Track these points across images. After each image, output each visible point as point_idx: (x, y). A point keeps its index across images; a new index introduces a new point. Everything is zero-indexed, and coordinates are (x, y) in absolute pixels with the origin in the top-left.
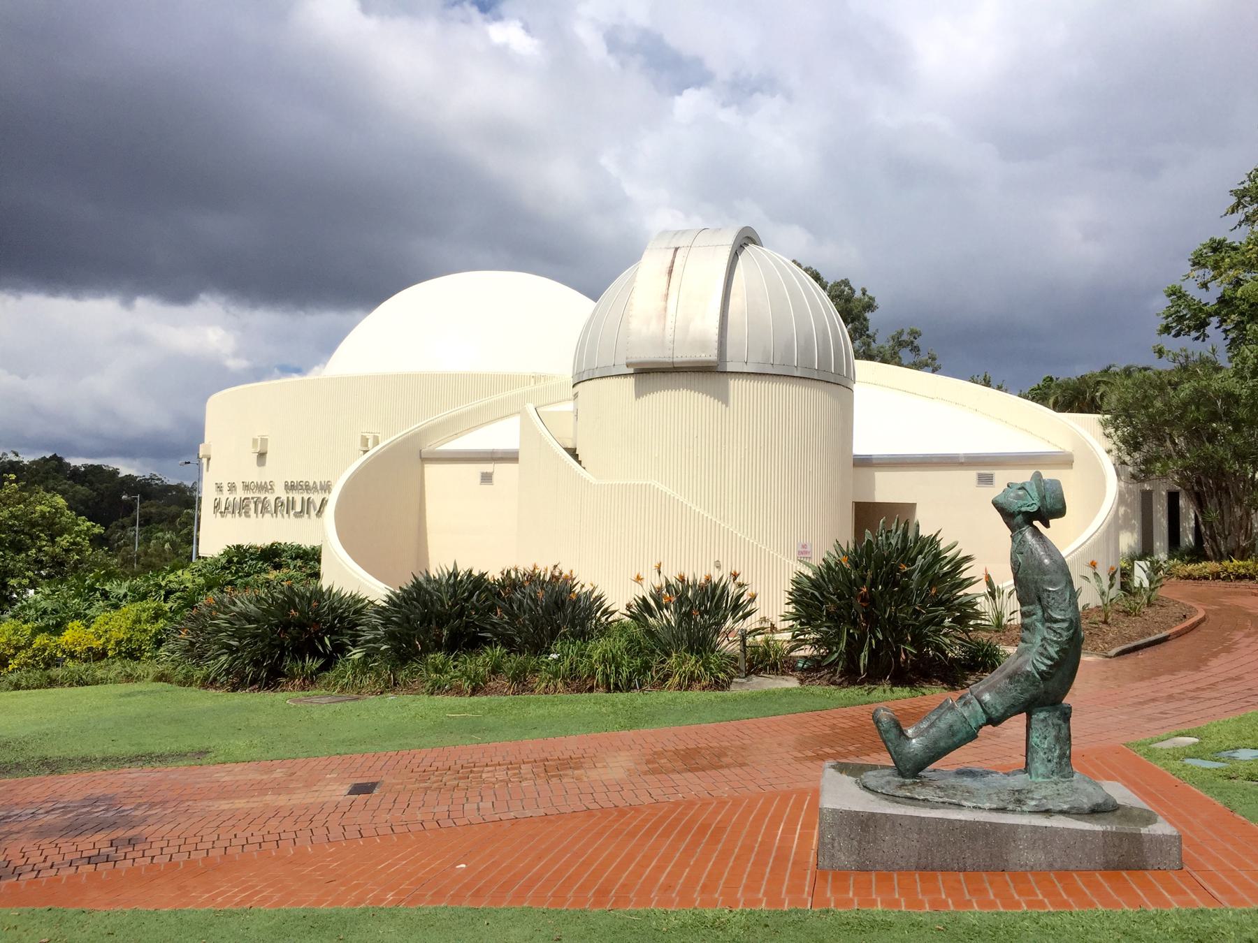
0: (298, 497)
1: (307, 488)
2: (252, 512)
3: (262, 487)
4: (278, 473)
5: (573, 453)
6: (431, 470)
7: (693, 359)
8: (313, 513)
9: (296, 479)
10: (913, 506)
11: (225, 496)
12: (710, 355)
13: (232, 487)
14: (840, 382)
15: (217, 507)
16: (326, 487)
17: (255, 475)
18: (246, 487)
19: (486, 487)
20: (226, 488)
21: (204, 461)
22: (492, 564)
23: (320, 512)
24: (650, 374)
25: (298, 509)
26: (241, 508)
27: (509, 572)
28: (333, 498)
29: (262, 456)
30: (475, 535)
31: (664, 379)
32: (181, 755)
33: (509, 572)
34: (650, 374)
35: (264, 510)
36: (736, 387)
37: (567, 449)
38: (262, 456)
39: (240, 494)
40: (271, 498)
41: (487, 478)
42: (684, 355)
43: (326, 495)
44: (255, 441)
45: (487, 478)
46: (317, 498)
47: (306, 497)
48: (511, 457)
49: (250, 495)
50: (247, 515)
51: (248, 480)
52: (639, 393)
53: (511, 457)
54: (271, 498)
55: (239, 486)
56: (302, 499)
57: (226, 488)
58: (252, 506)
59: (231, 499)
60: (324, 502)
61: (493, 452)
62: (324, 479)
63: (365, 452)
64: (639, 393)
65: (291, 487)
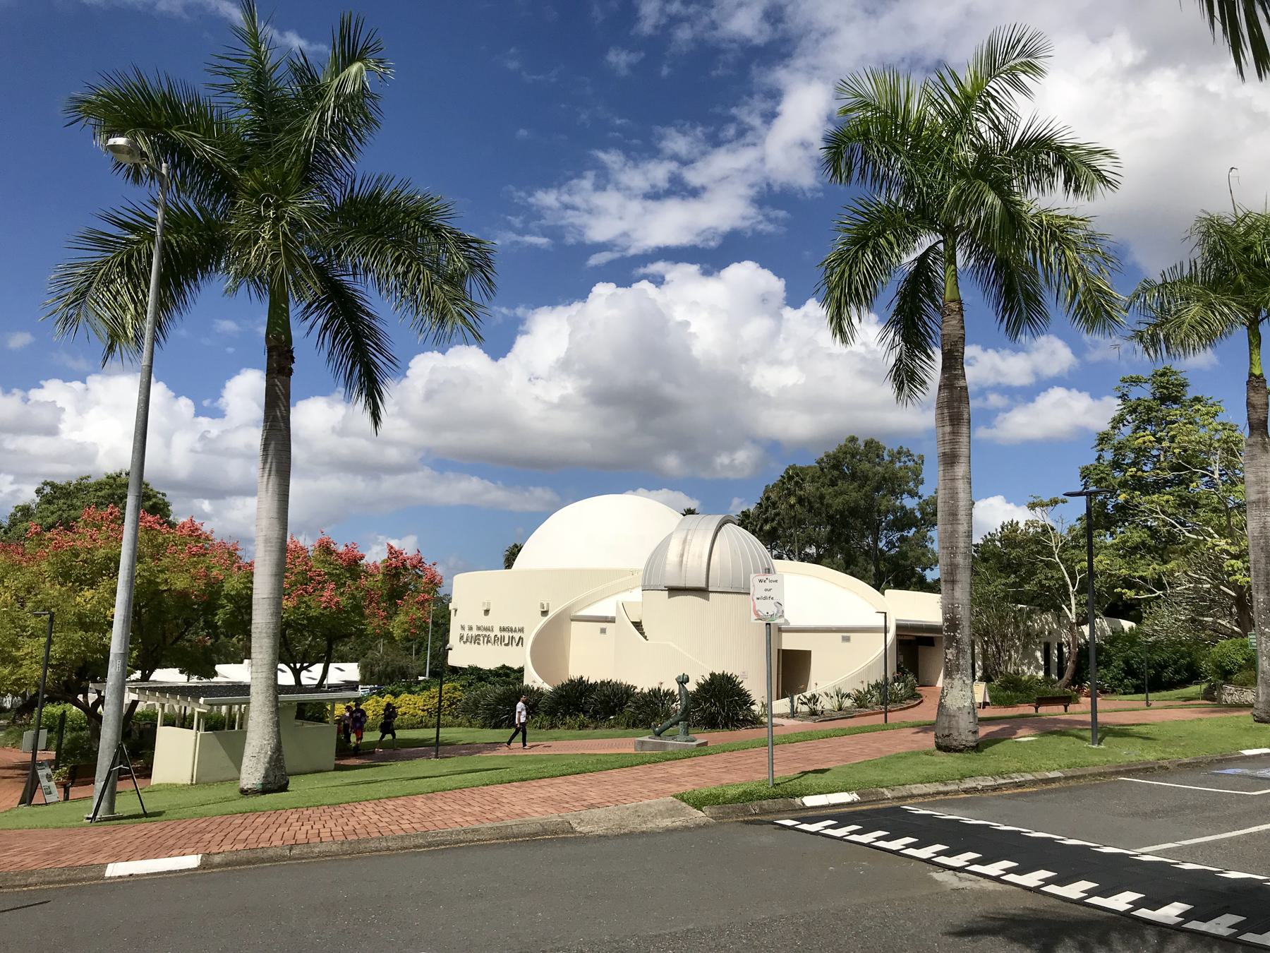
0: (506, 635)
1: (511, 630)
3: (487, 629)
4: (495, 621)
5: (638, 625)
6: (784, 635)
10: (810, 652)
11: (466, 633)
12: (703, 585)
13: (471, 628)
15: (461, 638)
16: (521, 630)
18: (479, 628)
19: (847, 644)
22: (593, 677)
24: (674, 591)
26: (476, 640)
29: (487, 612)
30: (590, 660)
34: (674, 591)
37: (633, 623)
38: (487, 612)
39: (475, 632)
40: (492, 635)
41: (603, 631)
42: (690, 584)
45: (603, 631)
46: (517, 636)
48: (612, 620)
53: (612, 620)
54: (492, 635)
56: (511, 637)
62: (518, 626)
65: (503, 629)
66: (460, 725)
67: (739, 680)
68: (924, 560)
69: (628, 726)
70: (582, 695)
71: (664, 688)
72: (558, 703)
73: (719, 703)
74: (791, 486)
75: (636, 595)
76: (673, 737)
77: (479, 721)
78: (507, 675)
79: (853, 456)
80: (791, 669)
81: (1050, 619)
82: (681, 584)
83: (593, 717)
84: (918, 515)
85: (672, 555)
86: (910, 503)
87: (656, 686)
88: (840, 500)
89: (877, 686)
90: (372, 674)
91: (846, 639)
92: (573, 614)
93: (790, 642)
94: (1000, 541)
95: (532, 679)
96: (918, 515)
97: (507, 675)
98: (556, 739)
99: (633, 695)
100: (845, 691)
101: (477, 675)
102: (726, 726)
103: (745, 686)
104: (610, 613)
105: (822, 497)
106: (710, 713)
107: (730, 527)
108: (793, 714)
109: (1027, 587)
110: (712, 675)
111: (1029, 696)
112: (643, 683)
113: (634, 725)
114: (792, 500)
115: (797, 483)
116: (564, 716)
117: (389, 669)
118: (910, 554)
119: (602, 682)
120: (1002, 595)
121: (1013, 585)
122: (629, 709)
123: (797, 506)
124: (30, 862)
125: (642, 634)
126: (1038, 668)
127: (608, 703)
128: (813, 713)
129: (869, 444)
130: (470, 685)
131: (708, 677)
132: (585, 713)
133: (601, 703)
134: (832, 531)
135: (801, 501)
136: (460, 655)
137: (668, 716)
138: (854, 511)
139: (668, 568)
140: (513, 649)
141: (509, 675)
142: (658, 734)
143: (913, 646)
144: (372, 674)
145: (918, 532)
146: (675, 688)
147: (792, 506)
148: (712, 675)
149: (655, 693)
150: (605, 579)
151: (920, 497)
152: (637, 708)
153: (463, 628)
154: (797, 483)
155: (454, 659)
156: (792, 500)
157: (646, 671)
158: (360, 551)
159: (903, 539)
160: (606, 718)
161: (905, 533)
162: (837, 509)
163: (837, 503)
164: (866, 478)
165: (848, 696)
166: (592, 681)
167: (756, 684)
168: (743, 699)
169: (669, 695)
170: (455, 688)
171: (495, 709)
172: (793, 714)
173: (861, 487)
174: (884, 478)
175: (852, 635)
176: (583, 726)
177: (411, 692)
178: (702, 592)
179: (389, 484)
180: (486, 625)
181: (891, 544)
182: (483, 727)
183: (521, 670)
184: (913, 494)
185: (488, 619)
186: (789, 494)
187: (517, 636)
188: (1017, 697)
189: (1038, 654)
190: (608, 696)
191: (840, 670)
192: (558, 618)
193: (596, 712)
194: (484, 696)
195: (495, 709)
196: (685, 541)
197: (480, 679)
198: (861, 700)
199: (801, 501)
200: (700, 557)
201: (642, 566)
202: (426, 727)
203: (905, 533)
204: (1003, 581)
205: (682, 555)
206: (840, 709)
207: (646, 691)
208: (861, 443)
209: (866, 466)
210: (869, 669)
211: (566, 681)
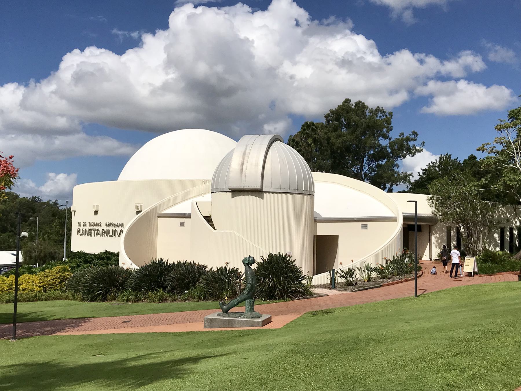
0: (111, 229)
1: (114, 225)
2: (93, 234)
3: (97, 225)
4: (102, 219)
5: (208, 219)
6: (318, 224)
7: (254, 187)
8: (117, 235)
9: (110, 222)
11: (82, 228)
12: (258, 186)
13: (85, 225)
14: (307, 192)
15: (79, 232)
16: (122, 225)
17: (96, 219)
18: (90, 224)
19: (182, 228)
20: (82, 225)
21: (73, 213)
23: (119, 236)
24: (236, 192)
25: (111, 234)
26: (88, 233)
27: (429, 164)
28: (125, 230)
29: (96, 212)
30: (172, 247)
31: (246, 193)
32: (212, 357)
33: (429, 164)
34: (236, 192)
35: (98, 234)
36: (265, 195)
37: (204, 217)
38: (96, 212)
39: (88, 227)
40: (100, 229)
43: (122, 228)
44: (94, 206)
45: (182, 224)
46: (119, 229)
47: (114, 229)
48: (189, 216)
49: (92, 228)
50: (91, 236)
51: (91, 222)
52: (233, 196)
53: (189, 216)
54: (100, 229)
55: (88, 224)
56: (112, 230)
57: (82, 225)
58: (93, 232)
59: (84, 229)
60: (121, 231)
61: (185, 214)
62: (121, 222)
63: (138, 212)
64: (233, 196)
65: (108, 225)
66: (66, 298)
67: (292, 259)
68: (393, 178)
69: (200, 299)
70: (162, 273)
71: (230, 267)
72: (141, 281)
73: (276, 279)
74: (309, 131)
75: (208, 197)
76: (240, 314)
77: (79, 295)
78: (109, 258)
79: (348, 112)
80: (324, 249)
81: (505, 211)
82: (242, 187)
83: (172, 291)
84: (389, 151)
85: (235, 164)
86: (384, 142)
87: (223, 265)
88: (340, 140)
89: (394, 261)
90: (31, 258)
91: (365, 227)
92: (159, 212)
93: (323, 230)
94: (438, 167)
95: (126, 263)
96: (389, 151)
97: (109, 258)
98: (137, 313)
99: (204, 273)
100: (373, 266)
101: (85, 258)
102: (282, 297)
103: (298, 264)
104: (187, 212)
105: (328, 139)
106: (269, 287)
107: (277, 143)
108: (333, 284)
109: (494, 187)
110: (270, 255)
111: (504, 267)
112: (213, 264)
113: (205, 298)
114: (310, 141)
115: (313, 129)
116: (147, 291)
117: (42, 255)
118: (385, 175)
119: (179, 263)
120: (475, 193)
121: (483, 187)
122: (201, 285)
123: (313, 145)
124: (24, 309)
125: (212, 225)
126: (496, 245)
127: (183, 280)
128: (349, 284)
129: (358, 104)
130: (78, 266)
131: (266, 257)
132: (164, 288)
133: (178, 280)
134: (334, 162)
135: (315, 141)
136: (79, 244)
137: (235, 294)
138: (348, 149)
139: (232, 174)
140: (115, 239)
141: (110, 258)
142: (226, 312)
143: (414, 229)
144: (31, 258)
145: (388, 161)
146: (242, 269)
147: (310, 145)
148: (270, 255)
149: (222, 271)
150: (183, 187)
151: (390, 139)
152: (208, 284)
153: (79, 224)
154: (313, 129)
155: (75, 248)
156: (310, 141)
157: (215, 253)
158: (20, 174)
159: (379, 166)
160: (182, 292)
161: (381, 162)
162: (346, 142)
163: (338, 142)
164: (357, 126)
165: (375, 270)
166: (170, 262)
167: (303, 261)
168: (296, 273)
169: (235, 272)
170: (65, 269)
171: (91, 287)
172: (333, 284)
173: (354, 132)
174: (368, 126)
175: (369, 224)
176: (162, 300)
177: (31, 273)
178: (258, 192)
179: (59, 142)
180: (96, 222)
181: (371, 169)
182: (83, 300)
183: (118, 255)
184: (385, 137)
185: (100, 216)
186: (308, 137)
187: (119, 229)
188: (496, 268)
189: (496, 235)
190: (184, 275)
191: (364, 250)
192: (148, 214)
193: (173, 288)
194: (83, 276)
195: (91, 287)
196: (244, 154)
197: (86, 262)
198: (382, 272)
199: (315, 141)
200: (257, 165)
201: (210, 177)
202: (39, 300)
203: (381, 162)
204: (476, 183)
205: (242, 165)
206: (369, 280)
207: (215, 269)
208: (353, 102)
209: (355, 118)
210: (387, 249)
211: (148, 262)
